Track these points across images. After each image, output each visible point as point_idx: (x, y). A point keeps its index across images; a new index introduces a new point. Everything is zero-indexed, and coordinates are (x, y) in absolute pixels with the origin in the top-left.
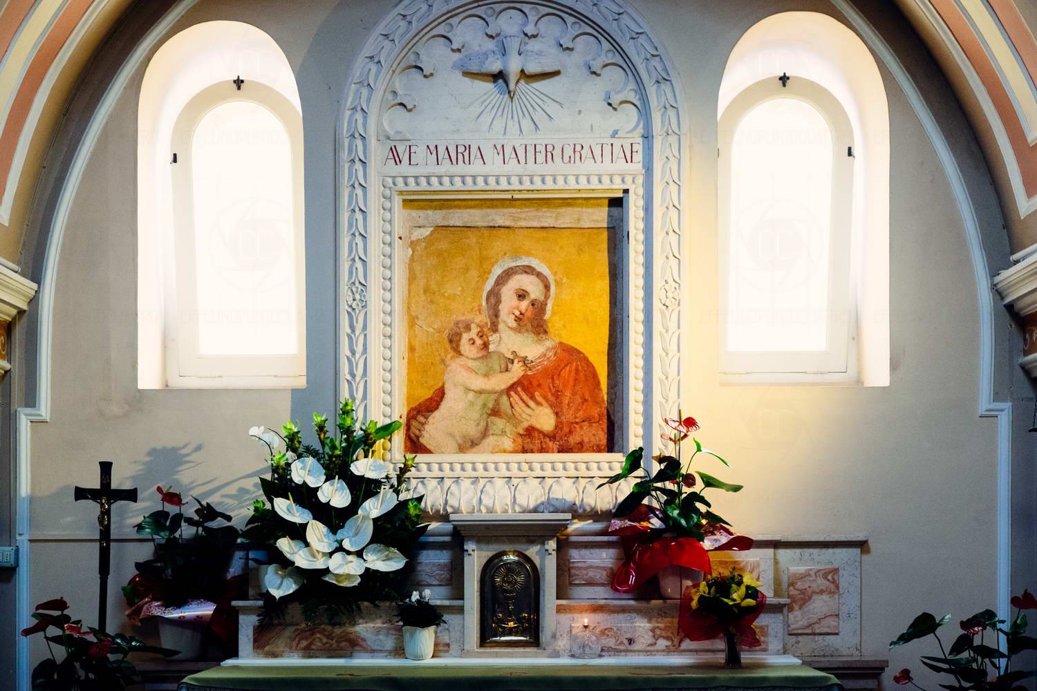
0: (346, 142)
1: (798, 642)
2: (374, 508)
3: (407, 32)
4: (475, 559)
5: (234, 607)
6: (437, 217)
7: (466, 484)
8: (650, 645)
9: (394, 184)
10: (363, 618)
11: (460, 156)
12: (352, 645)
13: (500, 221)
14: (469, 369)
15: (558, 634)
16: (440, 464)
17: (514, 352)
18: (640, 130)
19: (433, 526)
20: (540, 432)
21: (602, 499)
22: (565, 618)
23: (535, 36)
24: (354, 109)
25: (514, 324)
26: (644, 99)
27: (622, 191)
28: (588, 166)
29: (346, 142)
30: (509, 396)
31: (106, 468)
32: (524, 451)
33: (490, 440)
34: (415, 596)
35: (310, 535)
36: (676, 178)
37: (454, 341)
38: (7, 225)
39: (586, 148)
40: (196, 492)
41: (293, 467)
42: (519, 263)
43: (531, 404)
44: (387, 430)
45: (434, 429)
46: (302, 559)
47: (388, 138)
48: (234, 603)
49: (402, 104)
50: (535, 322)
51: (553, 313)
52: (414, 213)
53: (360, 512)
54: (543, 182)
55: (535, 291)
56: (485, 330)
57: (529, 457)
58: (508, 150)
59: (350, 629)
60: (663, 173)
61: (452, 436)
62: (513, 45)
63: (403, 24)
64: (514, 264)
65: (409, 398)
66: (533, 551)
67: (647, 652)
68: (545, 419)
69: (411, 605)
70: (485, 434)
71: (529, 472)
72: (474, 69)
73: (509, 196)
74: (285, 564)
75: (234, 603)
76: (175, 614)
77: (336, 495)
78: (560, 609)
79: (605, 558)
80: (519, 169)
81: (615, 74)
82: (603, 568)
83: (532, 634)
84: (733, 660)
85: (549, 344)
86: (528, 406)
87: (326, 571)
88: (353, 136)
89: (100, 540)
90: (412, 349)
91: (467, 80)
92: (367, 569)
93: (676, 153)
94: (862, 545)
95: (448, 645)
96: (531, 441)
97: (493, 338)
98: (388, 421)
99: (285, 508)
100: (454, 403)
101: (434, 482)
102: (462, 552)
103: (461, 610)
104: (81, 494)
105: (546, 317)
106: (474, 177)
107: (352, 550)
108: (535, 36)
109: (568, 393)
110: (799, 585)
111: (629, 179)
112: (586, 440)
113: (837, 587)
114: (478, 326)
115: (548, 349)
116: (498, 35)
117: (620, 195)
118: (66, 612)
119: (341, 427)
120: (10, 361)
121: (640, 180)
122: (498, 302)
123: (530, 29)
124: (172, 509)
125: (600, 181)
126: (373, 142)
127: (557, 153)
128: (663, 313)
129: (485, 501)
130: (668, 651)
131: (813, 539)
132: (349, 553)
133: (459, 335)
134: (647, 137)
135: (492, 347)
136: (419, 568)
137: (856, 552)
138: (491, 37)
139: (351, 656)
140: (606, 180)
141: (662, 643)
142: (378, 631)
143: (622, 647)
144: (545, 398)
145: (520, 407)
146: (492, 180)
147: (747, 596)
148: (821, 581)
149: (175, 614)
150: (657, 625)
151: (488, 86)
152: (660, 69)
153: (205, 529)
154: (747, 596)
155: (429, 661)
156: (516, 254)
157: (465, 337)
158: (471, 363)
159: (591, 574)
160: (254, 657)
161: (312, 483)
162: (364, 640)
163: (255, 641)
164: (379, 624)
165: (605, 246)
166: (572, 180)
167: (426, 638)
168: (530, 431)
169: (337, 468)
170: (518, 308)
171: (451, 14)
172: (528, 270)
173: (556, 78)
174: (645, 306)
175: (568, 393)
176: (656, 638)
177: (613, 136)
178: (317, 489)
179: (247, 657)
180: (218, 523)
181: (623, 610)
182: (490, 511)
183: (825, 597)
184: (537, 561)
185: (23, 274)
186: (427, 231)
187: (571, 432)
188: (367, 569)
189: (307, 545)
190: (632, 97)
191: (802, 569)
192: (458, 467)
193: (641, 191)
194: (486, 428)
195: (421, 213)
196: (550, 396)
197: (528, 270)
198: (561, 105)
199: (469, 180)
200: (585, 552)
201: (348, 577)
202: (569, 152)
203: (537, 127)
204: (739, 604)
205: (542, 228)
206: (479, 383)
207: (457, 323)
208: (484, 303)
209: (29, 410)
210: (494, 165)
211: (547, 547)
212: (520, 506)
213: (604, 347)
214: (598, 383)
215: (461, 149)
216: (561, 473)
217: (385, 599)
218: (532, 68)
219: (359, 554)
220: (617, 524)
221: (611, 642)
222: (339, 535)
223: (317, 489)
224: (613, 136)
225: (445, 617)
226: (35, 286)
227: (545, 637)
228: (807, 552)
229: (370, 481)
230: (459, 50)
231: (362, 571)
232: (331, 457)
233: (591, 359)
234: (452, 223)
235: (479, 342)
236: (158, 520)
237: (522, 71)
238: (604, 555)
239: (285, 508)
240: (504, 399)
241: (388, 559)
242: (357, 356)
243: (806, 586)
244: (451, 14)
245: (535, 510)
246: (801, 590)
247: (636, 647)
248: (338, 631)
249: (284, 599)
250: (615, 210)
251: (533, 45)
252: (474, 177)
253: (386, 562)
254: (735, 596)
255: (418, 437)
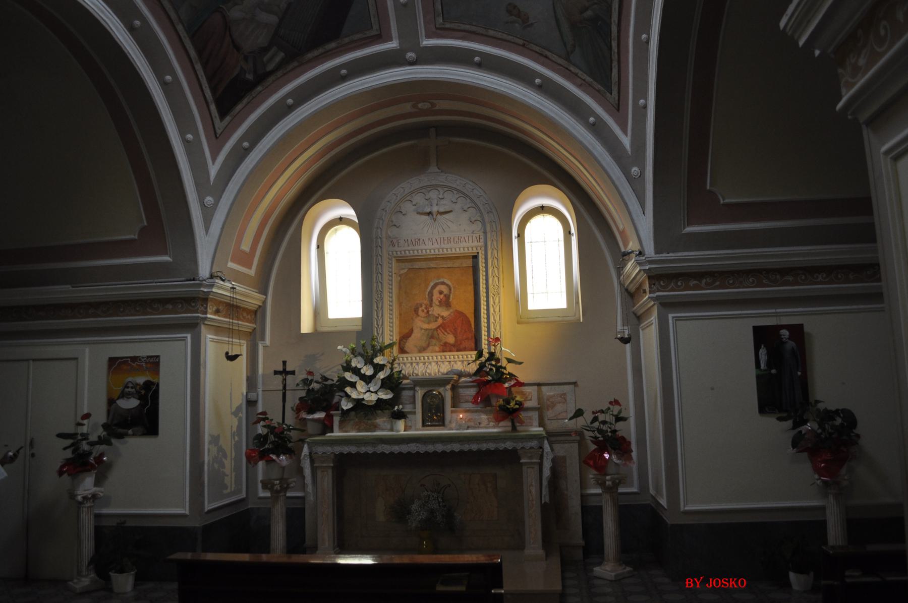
0: (375, 240)
1: (551, 423)
2: (382, 375)
3: (396, 199)
4: (420, 393)
5: (331, 414)
6: (409, 265)
7: (421, 365)
8: (487, 425)
9: (392, 254)
10: (378, 417)
11: (416, 243)
12: (375, 427)
13: (432, 266)
14: (422, 321)
15: (452, 422)
16: (411, 357)
17: (439, 314)
18: (482, 230)
19: (405, 381)
20: (449, 344)
21: (472, 369)
22: (454, 415)
23: (443, 199)
24: (377, 228)
25: (438, 304)
26: (483, 219)
27: (471, 257)
28: (464, 244)
29: (375, 240)
30: (437, 331)
31: (284, 363)
32: (443, 351)
33: (431, 348)
34: (396, 408)
35: (358, 386)
36: (496, 247)
37: (416, 311)
38: (253, 275)
39: (463, 237)
40: (321, 371)
41: (352, 361)
42: (440, 281)
43: (446, 333)
44: (391, 346)
45: (410, 344)
46: (354, 395)
47: (390, 237)
48: (331, 412)
49: (395, 225)
50: (446, 303)
51: (453, 299)
52: (400, 264)
53: (377, 376)
54: (447, 251)
55: (446, 291)
56: (428, 306)
57: (445, 354)
58: (434, 240)
59: (375, 421)
60: (491, 246)
61: (416, 347)
62: (435, 202)
63: (402, 190)
64: (438, 281)
65: (400, 333)
66: (441, 390)
67: (486, 428)
68: (451, 339)
69: (395, 411)
70: (428, 346)
71: (445, 360)
72: (421, 211)
73: (434, 256)
74: (348, 396)
75: (331, 412)
76: (311, 417)
77: (368, 371)
78: (452, 412)
79: (472, 392)
80: (438, 246)
81: (472, 211)
82: (471, 395)
83: (442, 422)
84: (514, 428)
85: (451, 310)
86: (444, 334)
87: (363, 399)
88: (377, 237)
89: (283, 390)
90: (400, 314)
91: (418, 216)
92: (379, 398)
93: (495, 238)
94: (575, 384)
95: (411, 426)
96: (446, 348)
97: (431, 309)
98: (391, 342)
99: (348, 376)
100: (417, 334)
101: (409, 365)
102: (415, 391)
103: (414, 413)
104: (276, 373)
105: (450, 301)
106: (422, 250)
107: (373, 391)
108: (443, 199)
109: (459, 329)
110: (551, 400)
111: (479, 248)
112: (467, 346)
113: (566, 401)
114: (425, 304)
115: (451, 313)
116: (430, 199)
117: (476, 254)
118: (267, 416)
119: (371, 345)
120: (256, 324)
121: (483, 249)
122: (432, 295)
123: (441, 196)
124: (310, 378)
125: (468, 250)
126: (384, 240)
127: (452, 240)
128: (493, 298)
129: (428, 371)
130: (494, 427)
131: (556, 382)
132: (372, 392)
133: (418, 308)
134: (485, 233)
135: (430, 313)
136: (402, 397)
137: (572, 387)
138: (427, 200)
139: (375, 431)
140: (470, 249)
141: (492, 424)
142: (384, 422)
143: (476, 426)
144: (451, 331)
145: (441, 335)
146: (428, 251)
147: (516, 404)
148: (559, 398)
149: (311, 417)
150: (489, 417)
151: (427, 217)
152: (488, 208)
153: (325, 385)
154: (516, 404)
155: (402, 432)
156: (439, 278)
157: (420, 309)
158: (422, 319)
159: (467, 398)
160: (339, 433)
161: (359, 366)
162: (379, 425)
163: (340, 426)
164: (385, 419)
165: (472, 273)
166: (458, 250)
167: (401, 424)
168: (446, 344)
169: (369, 361)
170: (439, 298)
171: (412, 193)
172: (443, 283)
173: (451, 213)
174: (486, 295)
175: (459, 329)
176: (489, 422)
177: (473, 233)
178: (361, 369)
179: (337, 433)
180: (329, 382)
181: (476, 411)
182: (430, 374)
183: (561, 404)
184: (443, 394)
185: (259, 293)
186: (406, 271)
187: (461, 343)
188: (379, 398)
189: (357, 390)
190: (479, 219)
191: (552, 394)
192: (418, 358)
193: (483, 252)
194: (429, 343)
195: (403, 264)
196: (452, 331)
197: (443, 283)
198: (453, 222)
199: (420, 251)
200: (464, 389)
201: (371, 401)
202: (456, 239)
203: (444, 231)
204: (512, 408)
205: (448, 268)
206: (426, 326)
207: (417, 304)
208: (427, 296)
209: (262, 342)
210: (429, 246)
211: (446, 388)
212: (441, 372)
213: (472, 311)
214: (471, 325)
215: (416, 241)
216: (457, 359)
217: (386, 409)
218: (442, 210)
219: (376, 392)
220: (474, 378)
221: (472, 424)
222: (369, 386)
223: (361, 369)
224: (473, 233)
225: (408, 416)
226: (265, 297)
227: (447, 422)
228: (553, 387)
229: (381, 365)
230: (415, 205)
231: (376, 399)
232: (366, 356)
233: (468, 315)
234: (414, 267)
235: (425, 311)
236: (306, 382)
237: (438, 211)
238: (472, 391)
239: (348, 376)
240: (435, 332)
241: (387, 394)
242: (379, 318)
243: (554, 400)
244: (412, 193)
245: (447, 374)
246: (551, 402)
247: (482, 425)
248: (369, 422)
249: (348, 410)
250: (475, 260)
251: (442, 202)
252: (422, 250)
253: (386, 396)
254: (511, 404)
255: (403, 348)
